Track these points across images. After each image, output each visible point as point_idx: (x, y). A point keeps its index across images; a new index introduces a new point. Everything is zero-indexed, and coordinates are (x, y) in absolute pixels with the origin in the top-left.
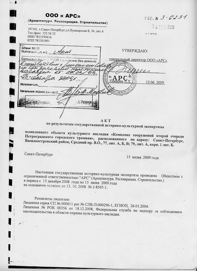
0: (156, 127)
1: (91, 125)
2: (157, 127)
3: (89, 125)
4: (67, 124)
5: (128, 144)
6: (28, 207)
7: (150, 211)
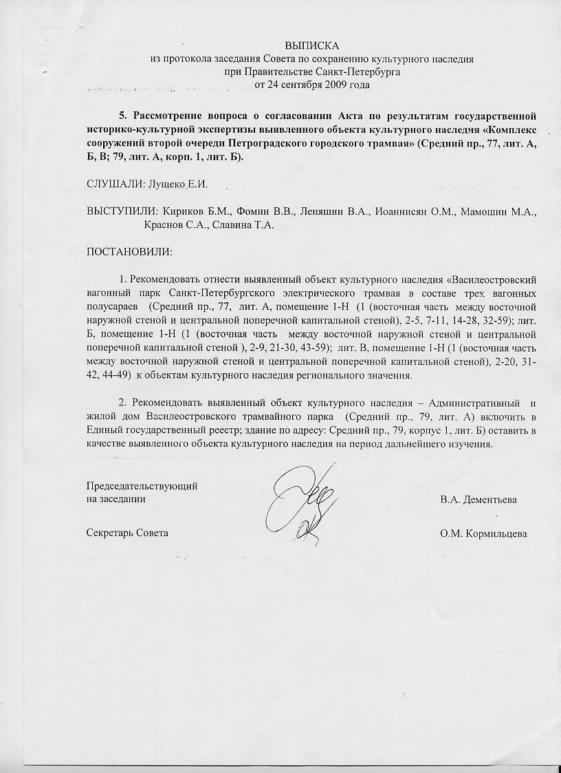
0: (232, 130)
1: (501, 117)
2: (236, 130)
3: (96, 130)
4: (431, 117)
5: (105, 158)
6: (317, 322)
7: (221, 60)
